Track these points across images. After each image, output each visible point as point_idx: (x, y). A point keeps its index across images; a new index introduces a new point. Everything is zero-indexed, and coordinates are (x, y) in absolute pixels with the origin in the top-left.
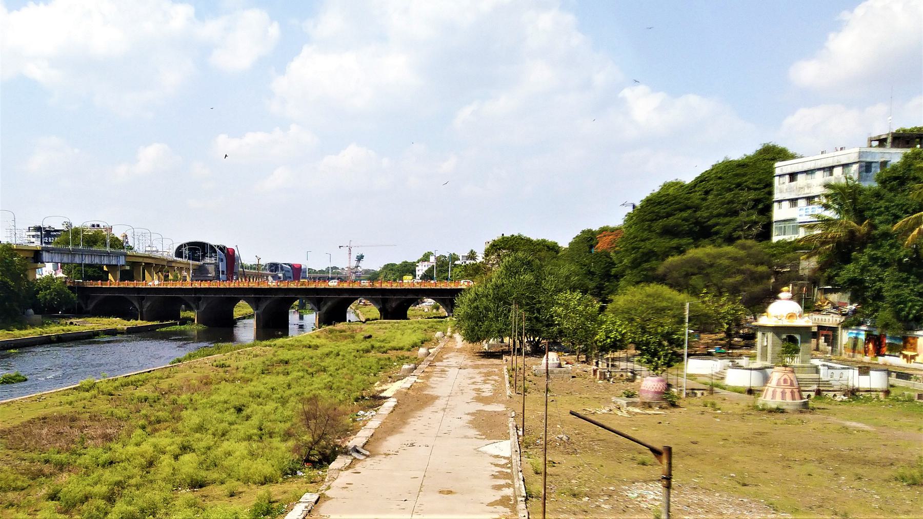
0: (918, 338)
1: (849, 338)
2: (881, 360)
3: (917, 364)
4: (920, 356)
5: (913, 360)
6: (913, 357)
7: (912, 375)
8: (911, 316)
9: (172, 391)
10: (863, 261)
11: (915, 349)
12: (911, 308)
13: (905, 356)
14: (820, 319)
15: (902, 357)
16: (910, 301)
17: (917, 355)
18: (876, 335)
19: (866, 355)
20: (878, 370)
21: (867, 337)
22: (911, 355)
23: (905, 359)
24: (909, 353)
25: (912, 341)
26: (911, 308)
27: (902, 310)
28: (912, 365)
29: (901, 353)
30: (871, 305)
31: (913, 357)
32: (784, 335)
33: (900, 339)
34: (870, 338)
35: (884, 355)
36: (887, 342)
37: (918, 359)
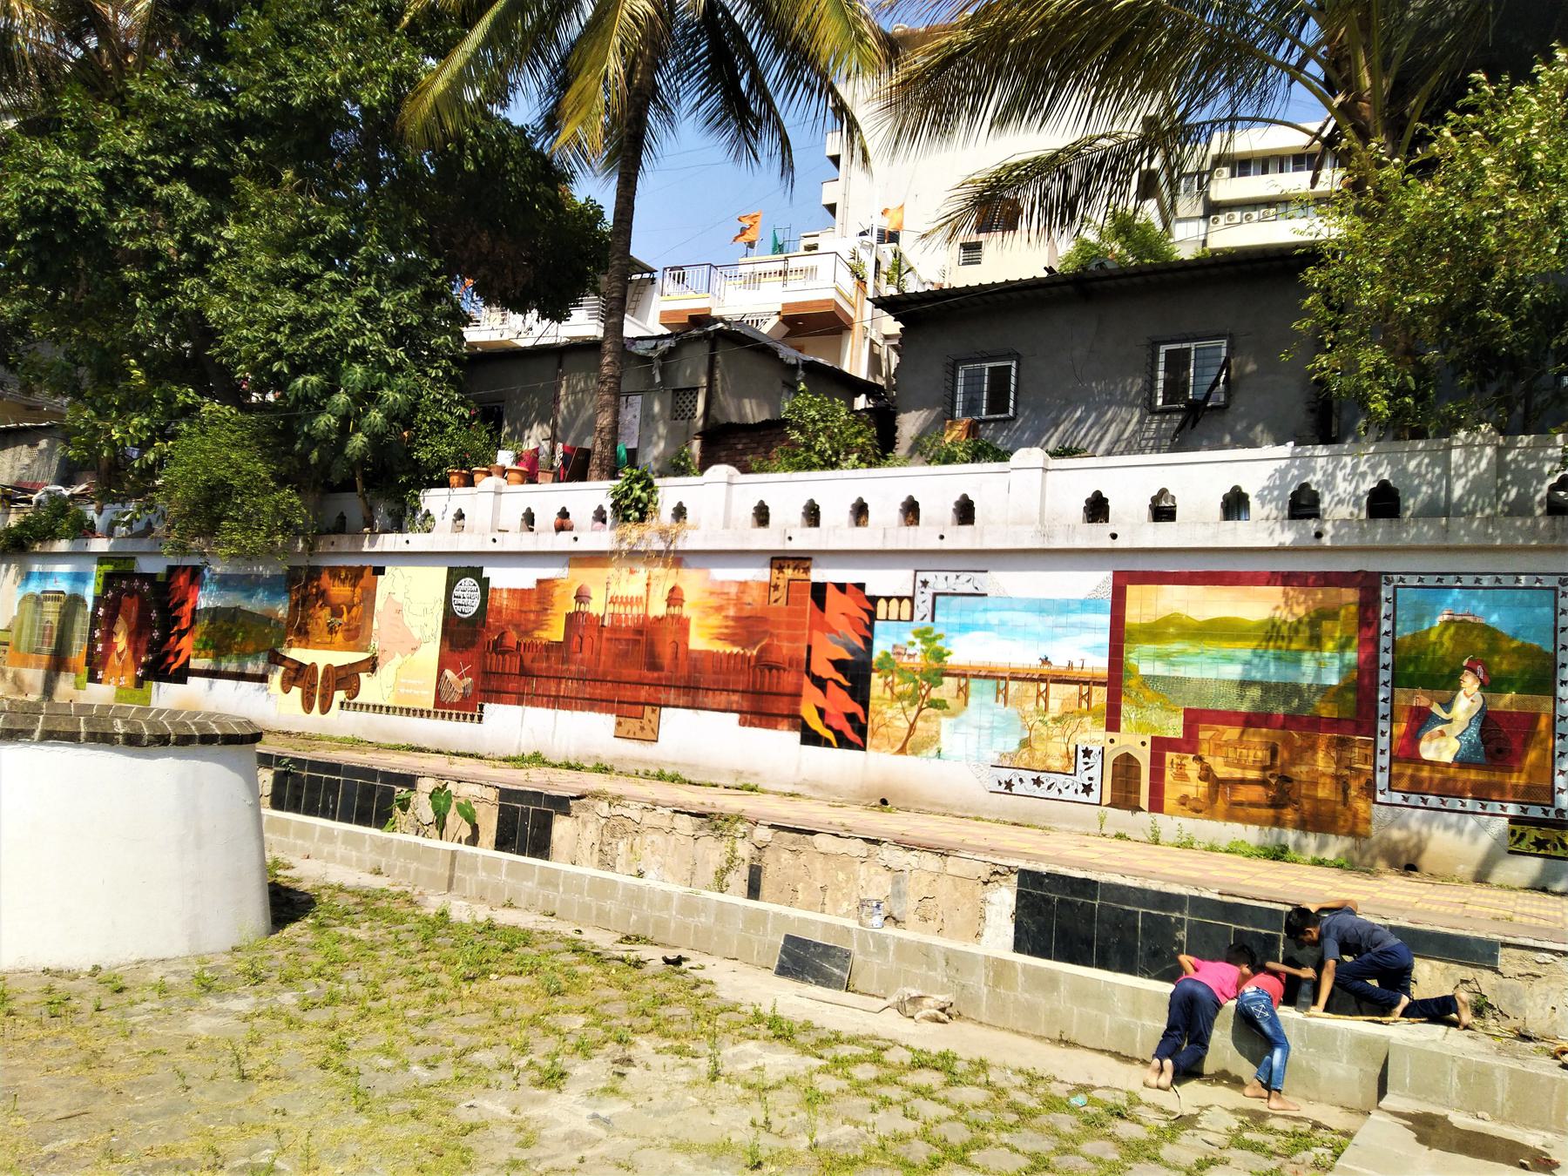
0: (380, 571)
1: (24, 599)
2: (166, 695)
3: (363, 715)
4: (386, 672)
5: (340, 696)
6: (345, 678)
7: (409, 781)
8: (358, 440)
9: (265, 973)
10: (1261, 36)
11: (355, 635)
12: (367, 396)
13: (299, 674)
14: (546, 518)
15: (276, 678)
16: (360, 354)
17: (372, 665)
18: (150, 578)
19: (93, 678)
20: (162, 740)
21: (105, 592)
22: (328, 668)
23: (296, 692)
24: (320, 658)
25: (339, 591)
26: (367, 396)
27: (313, 404)
28: (339, 720)
29: (276, 659)
30: (136, 402)
31: (345, 678)
32: (104, 613)
33: (274, 586)
34: (119, 593)
35: (181, 676)
36: (203, 603)
37: (371, 688)
